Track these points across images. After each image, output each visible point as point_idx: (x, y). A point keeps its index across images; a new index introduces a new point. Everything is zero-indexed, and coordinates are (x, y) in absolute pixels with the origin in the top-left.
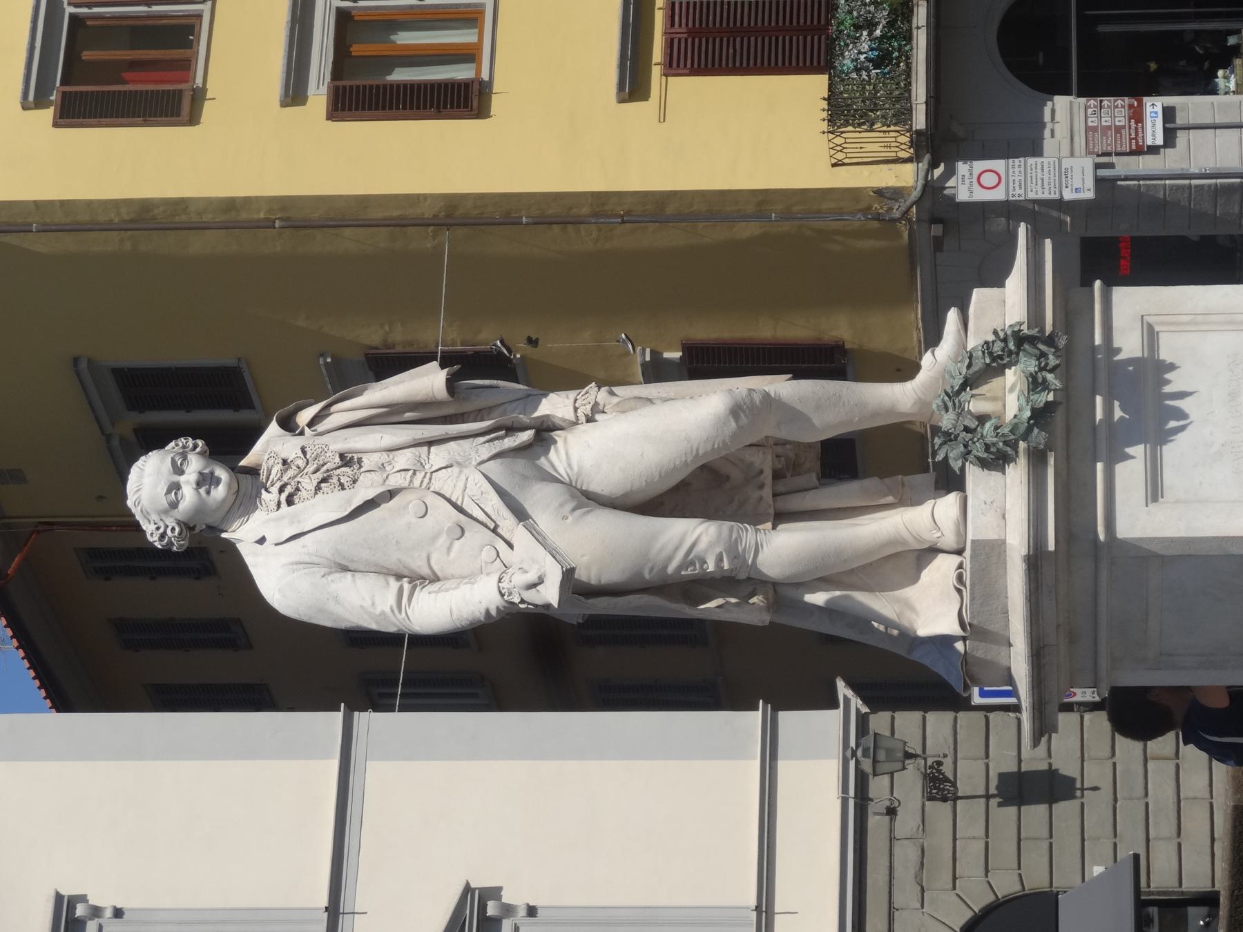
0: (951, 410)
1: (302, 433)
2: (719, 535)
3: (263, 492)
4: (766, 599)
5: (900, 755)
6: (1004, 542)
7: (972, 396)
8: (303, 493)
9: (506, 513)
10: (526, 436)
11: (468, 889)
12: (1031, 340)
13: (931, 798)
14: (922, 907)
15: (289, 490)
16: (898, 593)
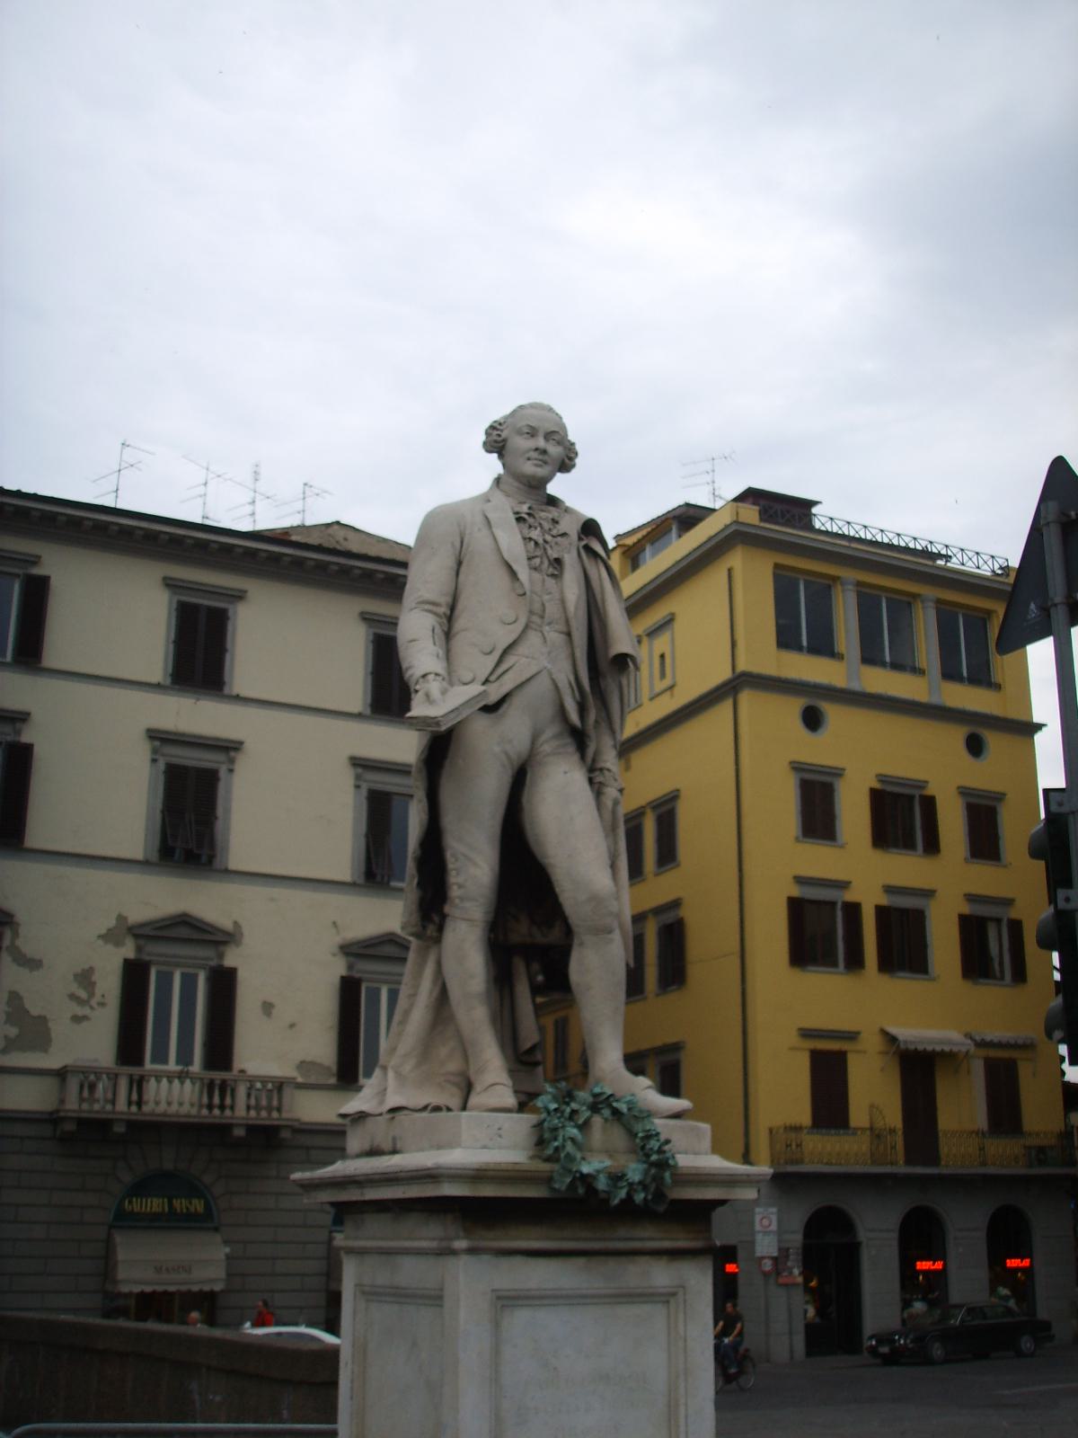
1: (580, 539)
10: (574, 717)
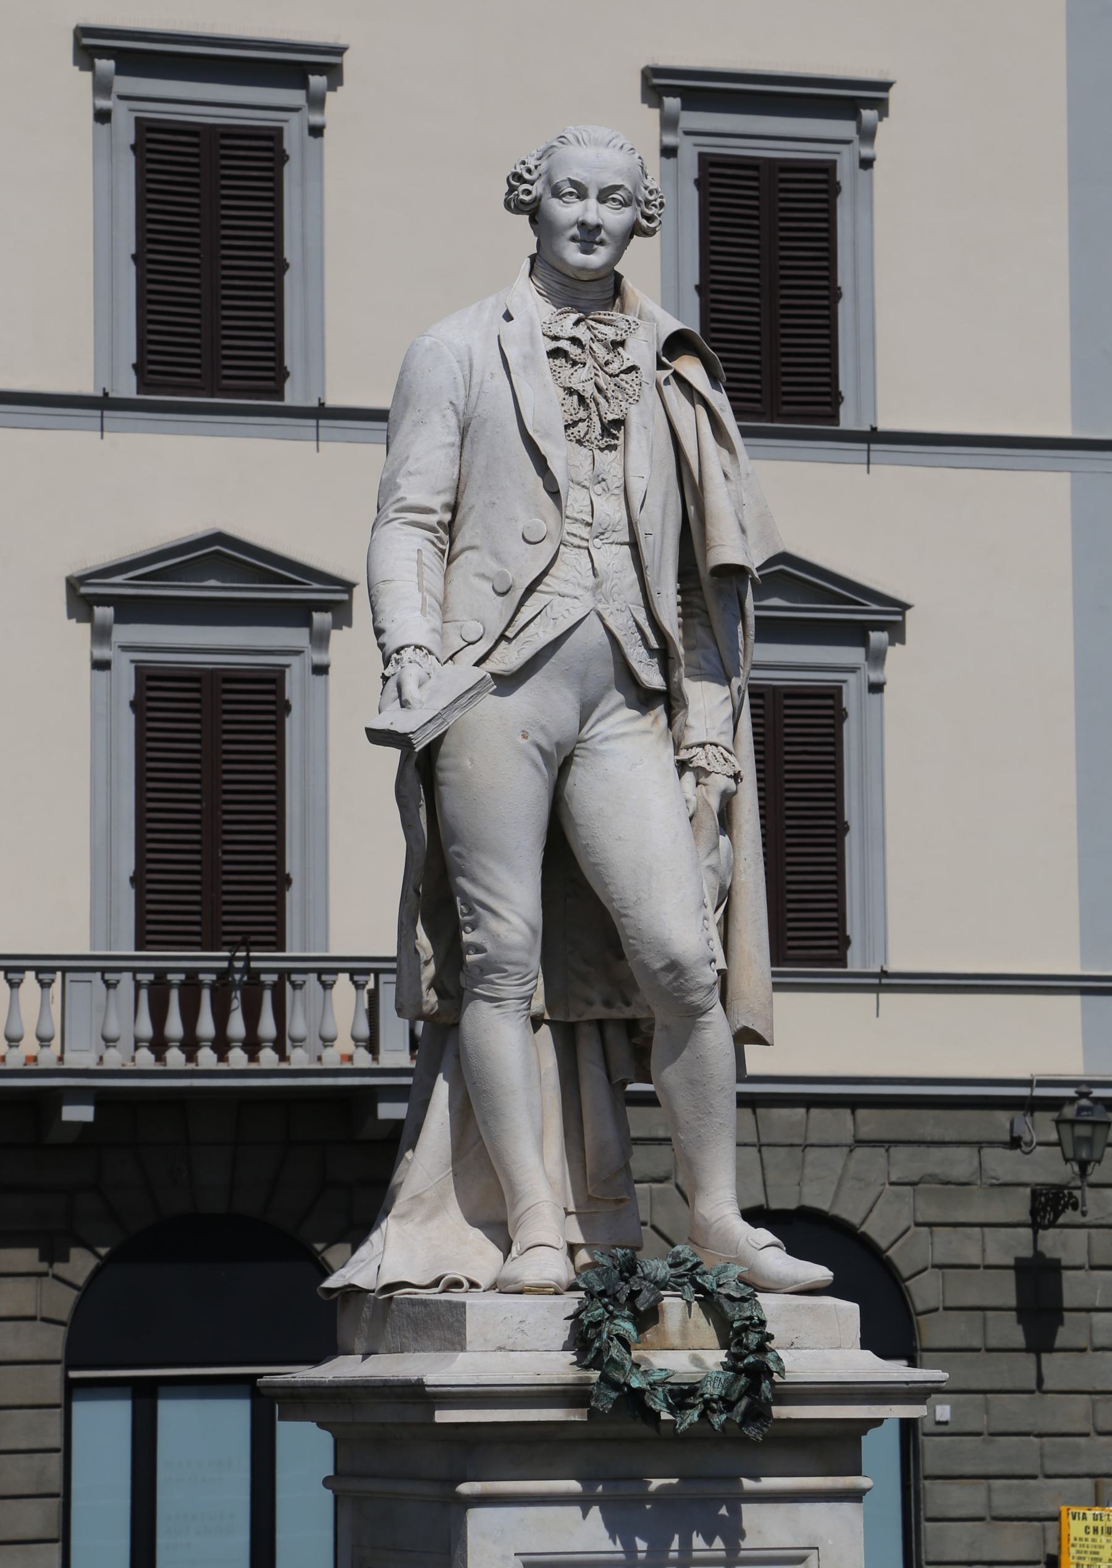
0: (673, 1271)
1: (661, 366)
2: (509, 948)
3: (574, 317)
4: (438, 1013)
5: (1084, 1155)
6: (463, 1349)
7: (689, 1303)
8: (567, 370)
9: (527, 653)
10: (652, 677)
11: (905, 607)
12: (753, 1389)
13: (1035, 1195)
14: (892, 1184)
15: (573, 351)
16: (453, 1194)
